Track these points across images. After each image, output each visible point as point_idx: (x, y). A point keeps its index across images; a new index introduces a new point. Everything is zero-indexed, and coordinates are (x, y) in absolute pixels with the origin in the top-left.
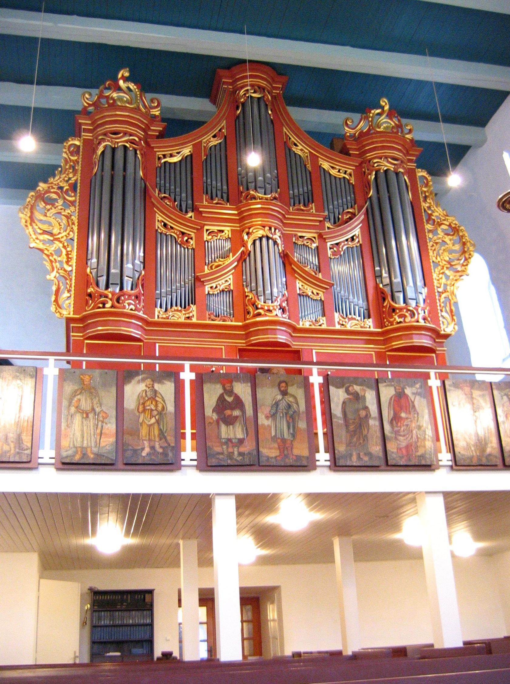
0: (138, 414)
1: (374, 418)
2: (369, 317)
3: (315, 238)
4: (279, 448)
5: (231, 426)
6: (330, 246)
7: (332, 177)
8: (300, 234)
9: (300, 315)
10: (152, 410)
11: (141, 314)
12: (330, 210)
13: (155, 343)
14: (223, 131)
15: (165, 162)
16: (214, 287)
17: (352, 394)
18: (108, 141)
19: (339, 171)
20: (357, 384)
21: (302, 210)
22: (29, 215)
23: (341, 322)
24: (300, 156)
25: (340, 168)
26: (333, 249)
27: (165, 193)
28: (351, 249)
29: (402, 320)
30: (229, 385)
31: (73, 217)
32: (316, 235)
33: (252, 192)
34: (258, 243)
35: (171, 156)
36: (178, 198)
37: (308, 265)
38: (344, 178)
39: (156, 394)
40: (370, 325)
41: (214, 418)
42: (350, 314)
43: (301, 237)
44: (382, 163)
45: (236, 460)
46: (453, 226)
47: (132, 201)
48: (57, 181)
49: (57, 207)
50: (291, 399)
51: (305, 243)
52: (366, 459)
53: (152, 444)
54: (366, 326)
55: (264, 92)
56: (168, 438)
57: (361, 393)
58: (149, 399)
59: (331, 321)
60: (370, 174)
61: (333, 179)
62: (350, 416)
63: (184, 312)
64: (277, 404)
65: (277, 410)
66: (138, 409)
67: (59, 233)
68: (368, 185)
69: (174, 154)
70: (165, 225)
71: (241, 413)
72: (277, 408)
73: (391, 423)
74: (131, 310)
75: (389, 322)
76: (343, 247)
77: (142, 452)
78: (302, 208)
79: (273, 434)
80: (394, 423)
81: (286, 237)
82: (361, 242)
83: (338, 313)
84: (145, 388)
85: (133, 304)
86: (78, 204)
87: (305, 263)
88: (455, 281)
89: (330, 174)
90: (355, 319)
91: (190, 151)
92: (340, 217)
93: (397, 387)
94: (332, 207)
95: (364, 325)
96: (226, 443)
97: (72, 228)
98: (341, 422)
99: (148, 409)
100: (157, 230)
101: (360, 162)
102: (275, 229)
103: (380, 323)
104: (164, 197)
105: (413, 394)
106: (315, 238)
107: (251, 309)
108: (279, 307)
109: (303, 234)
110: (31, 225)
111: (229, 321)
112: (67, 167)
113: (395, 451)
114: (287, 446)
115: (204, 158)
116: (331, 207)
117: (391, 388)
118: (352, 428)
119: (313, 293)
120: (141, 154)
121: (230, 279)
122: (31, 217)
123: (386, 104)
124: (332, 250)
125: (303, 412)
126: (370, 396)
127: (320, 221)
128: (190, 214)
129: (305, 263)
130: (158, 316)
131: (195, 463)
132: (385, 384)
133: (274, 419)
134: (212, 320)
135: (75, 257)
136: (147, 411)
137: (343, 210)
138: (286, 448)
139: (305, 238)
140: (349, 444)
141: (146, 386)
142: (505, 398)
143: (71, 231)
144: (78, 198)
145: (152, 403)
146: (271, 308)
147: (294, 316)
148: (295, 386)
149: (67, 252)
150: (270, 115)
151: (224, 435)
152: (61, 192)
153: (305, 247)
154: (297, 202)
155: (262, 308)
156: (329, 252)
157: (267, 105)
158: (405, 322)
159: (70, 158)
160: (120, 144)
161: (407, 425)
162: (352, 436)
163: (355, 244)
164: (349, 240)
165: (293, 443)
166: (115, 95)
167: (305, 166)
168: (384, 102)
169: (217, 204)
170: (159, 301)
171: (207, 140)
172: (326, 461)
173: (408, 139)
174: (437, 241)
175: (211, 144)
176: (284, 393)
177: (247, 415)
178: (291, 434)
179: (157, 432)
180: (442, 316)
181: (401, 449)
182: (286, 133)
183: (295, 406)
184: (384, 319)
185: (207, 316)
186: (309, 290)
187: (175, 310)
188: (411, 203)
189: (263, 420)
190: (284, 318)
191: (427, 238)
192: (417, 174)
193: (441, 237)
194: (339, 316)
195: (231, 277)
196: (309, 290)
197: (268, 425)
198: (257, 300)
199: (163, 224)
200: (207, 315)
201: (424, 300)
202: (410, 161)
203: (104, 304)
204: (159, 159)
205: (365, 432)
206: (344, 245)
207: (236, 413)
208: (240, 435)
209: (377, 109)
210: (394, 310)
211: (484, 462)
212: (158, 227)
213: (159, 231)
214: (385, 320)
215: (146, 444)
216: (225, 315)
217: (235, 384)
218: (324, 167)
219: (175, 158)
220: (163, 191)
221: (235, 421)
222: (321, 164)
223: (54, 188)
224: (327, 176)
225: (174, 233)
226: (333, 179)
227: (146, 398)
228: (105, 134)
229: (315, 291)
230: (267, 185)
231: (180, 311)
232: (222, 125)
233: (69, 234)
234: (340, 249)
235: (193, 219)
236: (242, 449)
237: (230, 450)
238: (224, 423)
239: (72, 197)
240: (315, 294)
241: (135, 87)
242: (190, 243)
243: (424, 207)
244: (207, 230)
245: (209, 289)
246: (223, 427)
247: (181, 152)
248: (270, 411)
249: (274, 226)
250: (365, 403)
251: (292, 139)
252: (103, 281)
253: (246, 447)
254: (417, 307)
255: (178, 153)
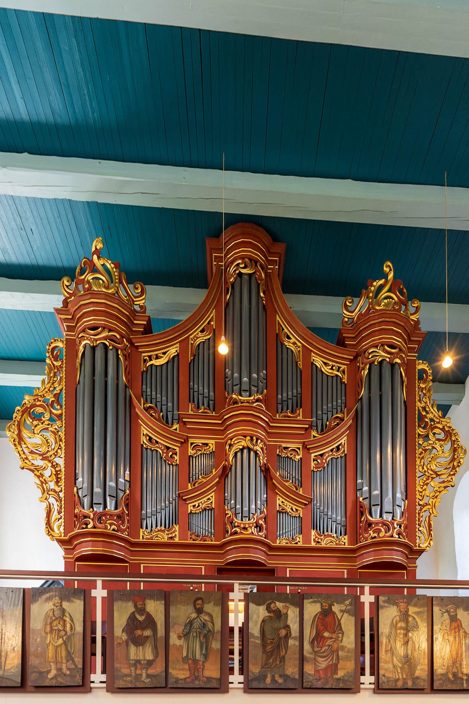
0: (44, 635)
1: (295, 638)
2: (345, 534)
3: (299, 449)
4: (190, 669)
5: (141, 647)
6: (314, 458)
7: (324, 375)
8: (284, 445)
9: (278, 533)
10: (59, 630)
11: (125, 535)
12: (318, 416)
13: (140, 564)
14: (212, 323)
15: (152, 365)
16: (197, 506)
17: (273, 611)
18: (87, 339)
19: (332, 369)
20: (280, 601)
21: (289, 417)
22: (16, 432)
23: (317, 539)
24: (292, 351)
25: (334, 364)
26: (317, 461)
27: (151, 403)
28: (335, 460)
29: (376, 535)
30: (141, 603)
31: (60, 433)
32: (300, 446)
33: (234, 396)
34: (239, 454)
35: (157, 357)
36: (164, 408)
37: (290, 479)
38: (337, 375)
39: (64, 612)
40: (345, 541)
41: (123, 638)
42: (327, 531)
43: (285, 448)
44: (378, 352)
45: (144, 682)
46: (447, 429)
47: (123, 414)
48: (42, 392)
49: (44, 422)
50: (207, 618)
51: (289, 455)
52: (280, 681)
53: (59, 666)
54: (341, 543)
55: (256, 266)
56: (76, 660)
57: (283, 611)
58: (57, 618)
59: (307, 539)
60: (363, 369)
61: (325, 377)
62: (268, 636)
63: (167, 532)
64: (191, 623)
65: (190, 630)
66: (45, 630)
67: (48, 451)
68: (360, 383)
69: (159, 355)
70: (150, 439)
71: (152, 634)
72: (191, 625)
73: (312, 643)
74: (114, 530)
75: (364, 538)
76: (327, 458)
77: (48, 674)
78: (289, 414)
79: (185, 655)
80: (316, 643)
81: (269, 450)
82: (346, 453)
83: (315, 530)
84: (53, 607)
85: (115, 525)
86: (64, 418)
87: (287, 478)
88: (438, 493)
89: (322, 372)
90: (330, 536)
91: (176, 351)
92: (328, 423)
93: (324, 604)
94: (321, 413)
95: (339, 542)
96: (135, 665)
97: (60, 445)
98: (259, 642)
99: (56, 630)
100: (142, 445)
101: (355, 354)
102: (257, 440)
103: (355, 539)
104: (150, 407)
105: (341, 611)
106: (299, 449)
107: (229, 527)
108: (255, 525)
109: (288, 445)
110: (20, 444)
111: (208, 541)
112: (51, 375)
113: (313, 672)
114: (198, 667)
115: (190, 358)
116: (319, 412)
117: (317, 604)
118: (269, 648)
119: (292, 509)
120: (124, 355)
121: (212, 497)
122: (19, 435)
123: (390, 270)
124: (315, 462)
125: (218, 632)
126: (292, 613)
127: (306, 429)
128: (176, 426)
129: (287, 478)
130: (143, 536)
131: (104, 685)
132: (311, 600)
133: (186, 640)
134: (194, 540)
135: (63, 477)
136: (54, 631)
137: (332, 416)
138: (196, 670)
139: (290, 449)
140: (265, 666)
141: (54, 605)
142: (446, 615)
143: (59, 448)
144: (64, 411)
145: (59, 623)
146: (247, 526)
147: (271, 534)
148: (212, 603)
149: (56, 471)
150: (262, 297)
151: (132, 656)
152: (47, 405)
153: (289, 459)
154: (285, 408)
155: (238, 526)
156: (313, 464)
157: (258, 285)
158: (379, 537)
159: (54, 364)
160: (98, 342)
161: (329, 645)
162: (268, 658)
163: (340, 454)
164: (334, 450)
165: (205, 664)
166: (90, 277)
167: (297, 363)
168: (388, 267)
169: (202, 412)
170: (145, 521)
171: (195, 336)
172: (239, 683)
173: (413, 320)
174: (427, 448)
175: (198, 341)
176: (200, 611)
177: (159, 636)
178: (204, 655)
179: (64, 653)
180: (419, 530)
181: (318, 671)
182: (279, 323)
183: (210, 625)
184: (360, 536)
185: (189, 536)
186: (288, 506)
187: (159, 531)
188: (405, 402)
189: (174, 640)
190: (261, 536)
191: (417, 444)
192: (417, 366)
193: (432, 443)
194: (316, 533)
195: (213, 494)
196: (288, 506)
197: (180, 646)
198: (234, 519)
199: (148, 438)
200: (189, 534)
201: (402, 514)
202: (410, 350)
203: (87, 524)
204: (145, 361)
205: (282, 654)
206: (329, 456)
207: (148, 633)
208: (149, 656)
209: (380, 279)
210: (370, 524)
211: (410, 684)
212: (144, 442)
213: (145, 446)
214: (361, 536)
215: (53, 666)
216: (207, 534)
217: (148, 601)
218: (316, 364)
219: (162, 359)
220: (149, 400)
221: (145, 642)
222: (314, 360)
223: (40, 401)
224: (319, 374)
225: (159, 447)
226: (325, 377)
227: (54, 618)
228: (84, 331)
229: (294, 507)
230: (253, 388)
231: (163, 531)
232: (211, 316)
233: (57, 452)
234: (324, 461)
235: (178, 431)
236: (150, 671)
237: (139, 672)
238: (133, 644)
239: (57, 410)
240: (294, 510)
241: (113, 266)
242: (174, 458)
243: (418, 408)
244: (192, 444)
245: (192, 508)
246: (133, 649)
247: (168, 351)
248: (183, 631)
249: (255, 435)
250: (287, 622)
251: (286, 330)
252: (86, 501)
253: (155, 668)
254: (393, 521)
255: (164, 353)
